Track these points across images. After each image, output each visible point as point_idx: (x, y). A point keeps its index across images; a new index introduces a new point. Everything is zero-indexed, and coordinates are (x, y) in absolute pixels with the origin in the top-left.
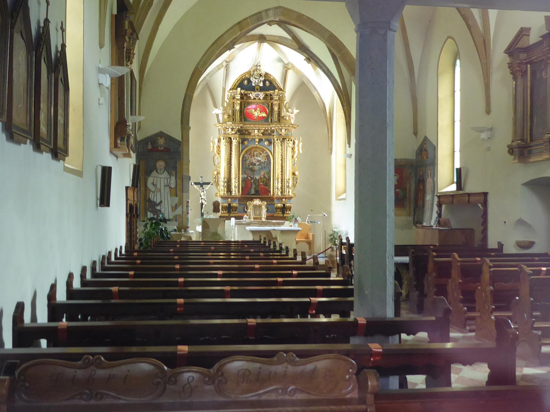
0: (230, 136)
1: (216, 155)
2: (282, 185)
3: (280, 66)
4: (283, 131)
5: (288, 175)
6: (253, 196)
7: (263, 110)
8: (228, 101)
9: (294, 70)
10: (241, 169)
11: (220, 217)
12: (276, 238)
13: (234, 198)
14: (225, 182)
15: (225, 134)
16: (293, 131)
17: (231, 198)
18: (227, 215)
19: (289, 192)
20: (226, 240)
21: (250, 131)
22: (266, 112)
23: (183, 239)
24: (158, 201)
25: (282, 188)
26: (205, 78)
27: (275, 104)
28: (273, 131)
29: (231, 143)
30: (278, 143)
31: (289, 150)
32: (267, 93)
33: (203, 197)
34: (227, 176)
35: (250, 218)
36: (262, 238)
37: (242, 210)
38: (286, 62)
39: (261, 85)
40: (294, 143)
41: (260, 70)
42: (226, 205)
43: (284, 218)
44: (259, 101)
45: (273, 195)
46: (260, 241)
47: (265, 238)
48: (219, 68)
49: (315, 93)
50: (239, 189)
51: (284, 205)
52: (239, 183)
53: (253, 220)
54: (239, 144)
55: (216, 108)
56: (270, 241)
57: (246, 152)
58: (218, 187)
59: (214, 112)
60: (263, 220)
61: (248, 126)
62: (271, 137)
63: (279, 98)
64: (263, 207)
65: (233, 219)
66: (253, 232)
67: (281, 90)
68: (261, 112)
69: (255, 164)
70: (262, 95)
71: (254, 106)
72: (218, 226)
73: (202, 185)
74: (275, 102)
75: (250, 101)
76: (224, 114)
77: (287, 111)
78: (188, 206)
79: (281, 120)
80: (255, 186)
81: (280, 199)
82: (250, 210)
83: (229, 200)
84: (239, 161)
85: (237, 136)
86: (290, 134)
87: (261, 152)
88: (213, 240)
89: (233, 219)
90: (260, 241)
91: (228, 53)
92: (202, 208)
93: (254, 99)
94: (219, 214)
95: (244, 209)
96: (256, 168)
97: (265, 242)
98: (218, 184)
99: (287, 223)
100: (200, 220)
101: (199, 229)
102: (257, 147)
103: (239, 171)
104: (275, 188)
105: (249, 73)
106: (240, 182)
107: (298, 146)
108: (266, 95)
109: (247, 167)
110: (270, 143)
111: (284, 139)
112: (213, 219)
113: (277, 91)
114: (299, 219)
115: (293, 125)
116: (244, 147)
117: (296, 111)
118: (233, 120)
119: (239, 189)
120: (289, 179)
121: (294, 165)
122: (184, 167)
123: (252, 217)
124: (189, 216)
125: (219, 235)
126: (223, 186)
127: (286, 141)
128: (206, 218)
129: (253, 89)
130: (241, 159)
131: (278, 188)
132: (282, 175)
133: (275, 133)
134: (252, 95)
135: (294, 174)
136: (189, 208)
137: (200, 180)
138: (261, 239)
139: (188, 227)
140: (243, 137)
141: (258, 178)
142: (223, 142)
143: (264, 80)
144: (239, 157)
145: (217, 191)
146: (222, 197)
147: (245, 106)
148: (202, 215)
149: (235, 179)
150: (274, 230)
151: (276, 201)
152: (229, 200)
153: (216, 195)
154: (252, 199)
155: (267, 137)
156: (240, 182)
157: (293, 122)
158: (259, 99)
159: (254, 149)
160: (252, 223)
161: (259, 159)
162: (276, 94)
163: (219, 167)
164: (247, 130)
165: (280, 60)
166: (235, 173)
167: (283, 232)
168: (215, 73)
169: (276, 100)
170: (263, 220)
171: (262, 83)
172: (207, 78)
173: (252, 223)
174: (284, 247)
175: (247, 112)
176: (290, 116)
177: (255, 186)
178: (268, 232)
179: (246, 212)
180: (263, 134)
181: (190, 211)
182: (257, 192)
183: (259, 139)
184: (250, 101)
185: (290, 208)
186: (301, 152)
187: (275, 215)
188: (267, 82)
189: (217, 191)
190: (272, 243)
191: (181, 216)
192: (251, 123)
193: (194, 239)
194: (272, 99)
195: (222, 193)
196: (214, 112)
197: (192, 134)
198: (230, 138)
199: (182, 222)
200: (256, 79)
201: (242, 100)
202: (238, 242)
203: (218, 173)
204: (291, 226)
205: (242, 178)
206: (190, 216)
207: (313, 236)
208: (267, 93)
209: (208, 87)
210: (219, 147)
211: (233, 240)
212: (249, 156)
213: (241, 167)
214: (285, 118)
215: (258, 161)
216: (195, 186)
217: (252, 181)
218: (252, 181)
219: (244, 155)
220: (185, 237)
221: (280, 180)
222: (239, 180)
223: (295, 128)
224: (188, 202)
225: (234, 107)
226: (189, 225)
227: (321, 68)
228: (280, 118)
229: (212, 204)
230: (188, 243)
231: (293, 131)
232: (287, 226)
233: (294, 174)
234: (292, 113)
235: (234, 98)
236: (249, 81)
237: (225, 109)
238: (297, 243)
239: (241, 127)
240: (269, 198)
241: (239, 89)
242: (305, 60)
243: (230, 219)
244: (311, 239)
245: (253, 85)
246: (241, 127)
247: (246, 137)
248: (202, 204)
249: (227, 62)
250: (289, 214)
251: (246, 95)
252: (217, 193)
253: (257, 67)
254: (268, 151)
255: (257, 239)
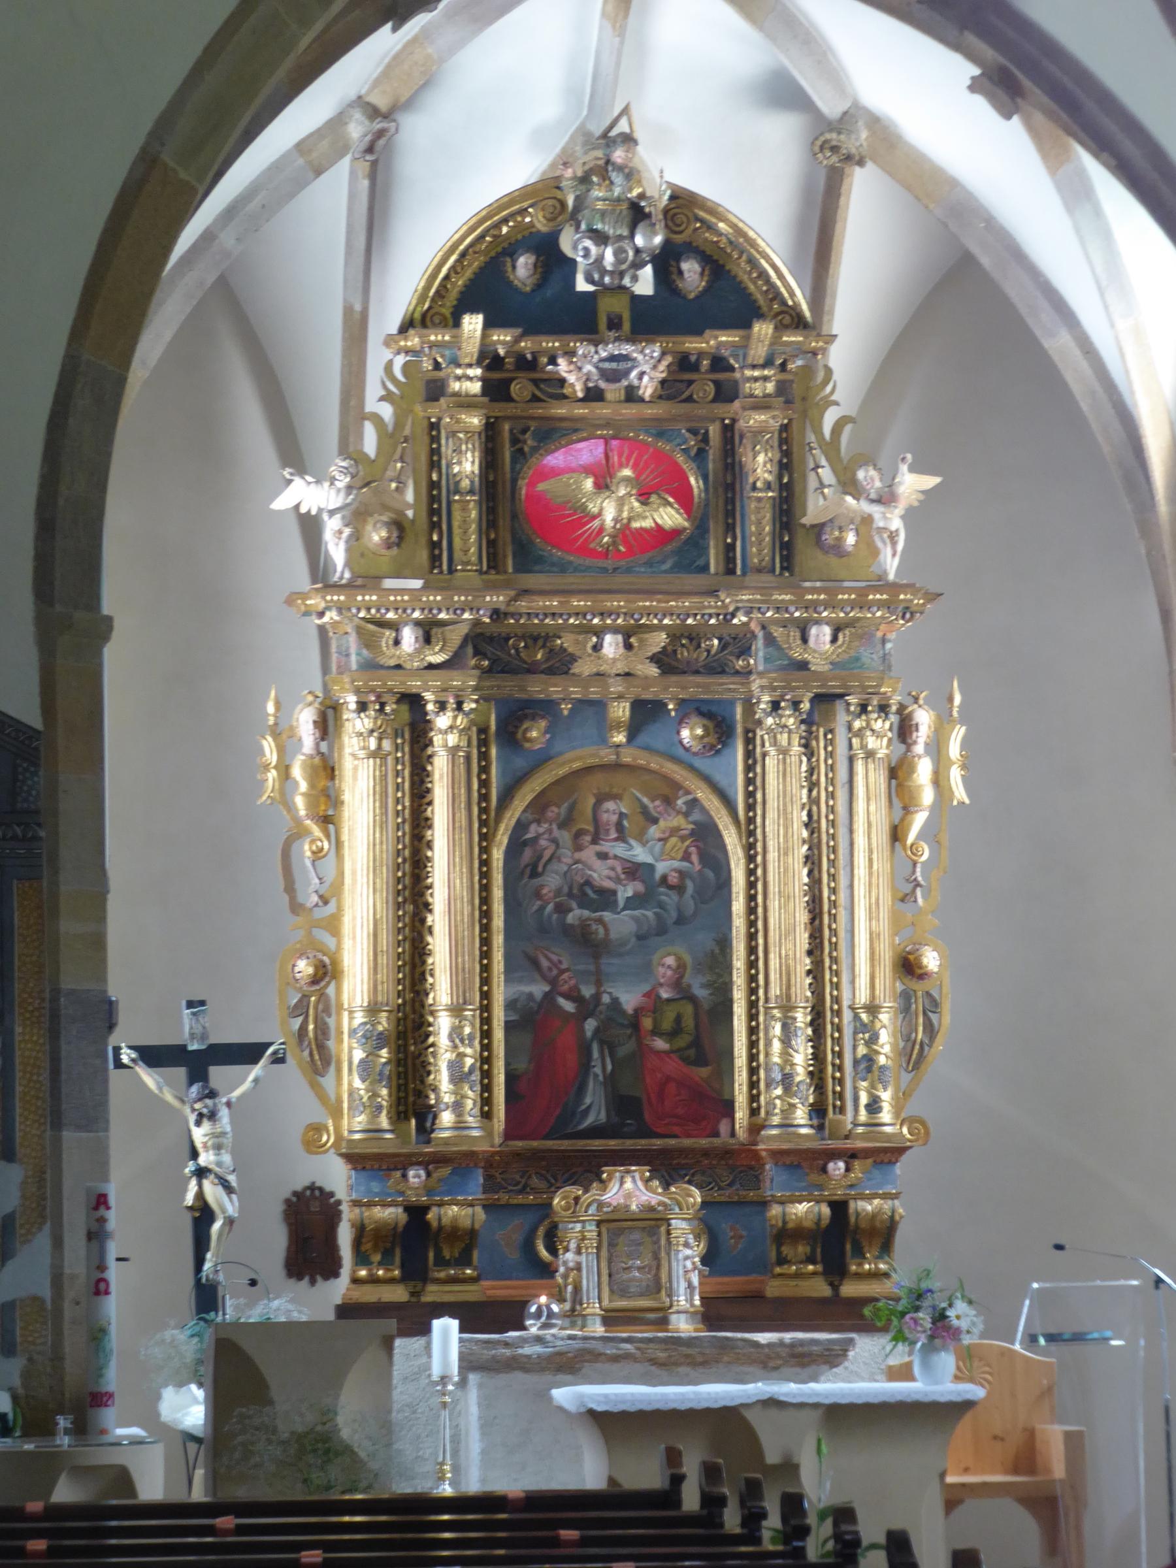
0: (414, 685)
1: (298, 833)
2: (818, 1057)
3: (779, 139)
4: (821, 635)
5: (865, 976)
6: (597, 1144)
7: (659, 482)
8: (386, 411)
9: (889, 169)
10: (498, 940)
11: (346, 1311)
12: (789, 1468)
13: (453, 1163)
14: (381, 1040)
15: (371, 666)
16: (897, 635)
17: (430, 1162)
18: (398, 1294)
19: (880, 1108)
20: (404, 1487)
21: (566, 642)
22: (684, 498)
23: (65, 1493)
24: (668, 1304)
25: (817, 1076)
26: (208, 237)
27: (758, 432)
28: (739, 644)
29: (417, 734)
30: (780, 735)
31: (870, 781)
32: (693, 345)
33: (205, 1159)
34: (389, 993)
35: (574, 1315)
36: (691, 1467)
37: (514, 1255)
38: (830, 107)
39: (645, 283)
40: (905, 730)
41: (631, 174)
42: (391, 1214)
43: (853, 1316)
44: (630, 411)
45: (755, 1129)
46: (669, 1497)
47: (711, 1472)
48: (313, 156)
49: (1058, 344)
50: (487, 1088)
51: (839, 1208)
52: (487, 1047)
53: (598, 1329)
54: (483, 743)
55: (301, 471)
56: (752, 1490)
57: (539, 805)
58: (328, 1082)
59: (283, 502)
60: (683, 1326)
61: (543, 607)
62: (721, 688)
63: (782, 389)
64: (680, 1226)
65: (446, 1329)
66: (609, 1424)
67: (797, 322)
68: (644, 496)
69: (606, 898)
70: (648, 366)
71: (588, 451)
72: (335, 1383)
73: (197, 1063)
74: (757, 419)
75: (560, 410)
76: (357, 517)
77: (850, 485)
78: (97, 1235)
79: (806, 555)
80: (603, 1056)
81: (806, 1162)
82: (579, 1254)
83: (416, 1176)
84: (485, 875)
85: (465, 680)
86: (870, 657)
87: (654, 806)
88: (298, 1494)
89: (446, 1329)
90: (669, 1497)
91: (383, 43)
92: (201, 1244)
93: (594, 395)
94: (339, 1289)
95: (528, 1246)
96: (620, 924)
97: (713, 1502)
98: (320, 1056)
99: (867, 1348)
100: (184, 1339)
101: (188, 1408)
102: (617, 766)
103: (486, 954)
104: (771, 1075)
105: (544, 191)
106: (499, 1034)
107: (937, 749)
108: (684, 364)
109: (539, 916)
110: (721, 729)
111: (825, 700)
112: (291, 1326)
113: (763, 330)
114: (961, 1314)
115: (894, 588)
116: (520, 763)
117: (912, 484)
118: (435, 560)
119: (487, 1088)
120: (873, 1009)
121: (905, 898)
122: (68, 926)
123: (594, 1308)
124: (113, 1307)
125: (347, 1450)
126: (366, 1068)
127: (842, 718)
128: (236, 1325)
129: (580, 319)
130: (498, 855)
131: (787, 1080)
132: (816, 973)
133: (757, 659)
134: (577, 366)
135: (908, 966)
136: (113, 1250)
137: (185, 1030)
138: (677, 1480)
139: (100, 1399)
140: (509, 686)
141: (630, 998)
142: (357, 728)
143: (667, 243)
144: (486, 839)
145: (315, 1113)
146: (357, 1160)
147: (520, 455)
148: (207, 1297)
149: (456, 1010)
150: (772, 1403)
151: (774, 1180)
152: (416, 1176)
153: (312, 1141)
154: (587, 1170)
155: (694, 687)
156: (499, 1034)
157: (891, 564)
158: (631, 395)
159: (597, 782)
160: (596, 1356)
161: (640, 854)
162: (759, 352)
163: (333, 925)
164: (538, 638)
165: (782, 93)
166: (456, 971)
167: (841, 1417)
168: (292, 195)
169: (762, 405)
170: (683, 1326)
171: (648, 271)
172: (227, 239)
173: (596, 1356)
174: (871, 1530)
175: (537, 499)
176: (868, 520)
177: (603, 1056)
178: (727, 1422)
179: (546, 1271)
180: (665, 662)
181: (114, 1273)
182: (628, 1114)
183: (639, 706)
184: (560, 410)
185: (883, 1235)
186: (960, 793)
187: (774, 1289)
188: (690, 268)
189: (315, 1113)
190: (772, 1507)
191: (50, 1313)
192: (570, 580)
193: (152, 1488)
194: (726, 393)
195: (355, 1124)
196: (283, 502)
197: (125, 673)
198: (414, 701)
199: (57, 1357)
200: (601, 238)
201: (501, 409)
202: (488, 1502)
203: (327, 972)
204: (903, 1373)
205: (510, 1005)
206: (113, 1309)
207: (1074, 1442)
208: (693, 345)
209: (237, 312)
210: (326, 769)
211: (447, 1490)
212: (565, 837)
213: (498, 922)
214: (829, 537)
215: (634, 870)
216: (148, 1078)
217: (590, 1025)
218: (590, 1025)
219: (520, 827)
220: (82, 1472)
221: (802, 1018)
222: (486, 1021)
223: (908, 612)
224: (101, 1201)
225: (434, 460)
226: (113, 1379)
227: (1102, 147)
228: (794, 540)
229: (277, 1209)
230: (113, 1517)
231: (897, 635)
232: (866, 1372)
233: (908, 966)
234: (886, 498)
235: (435, 390)
236: (553, 261)
237: (366, 477)
238: (953, 1499)
239: (496, 614)
240: (727, 1154)
241: (473, 323)
242: (975, 86)
243: (426, 1330)
244: (1059, 1471)
245: (582, 285)
246: (496, 614)
247: (537, 688)
248: (203, 1214)
249: (374, 112)
250: (898, 1272)
251: (527, 364)
252: (319, 1129)
253: (606, 148)
254: (703, 794)
255: (645, 1474)
